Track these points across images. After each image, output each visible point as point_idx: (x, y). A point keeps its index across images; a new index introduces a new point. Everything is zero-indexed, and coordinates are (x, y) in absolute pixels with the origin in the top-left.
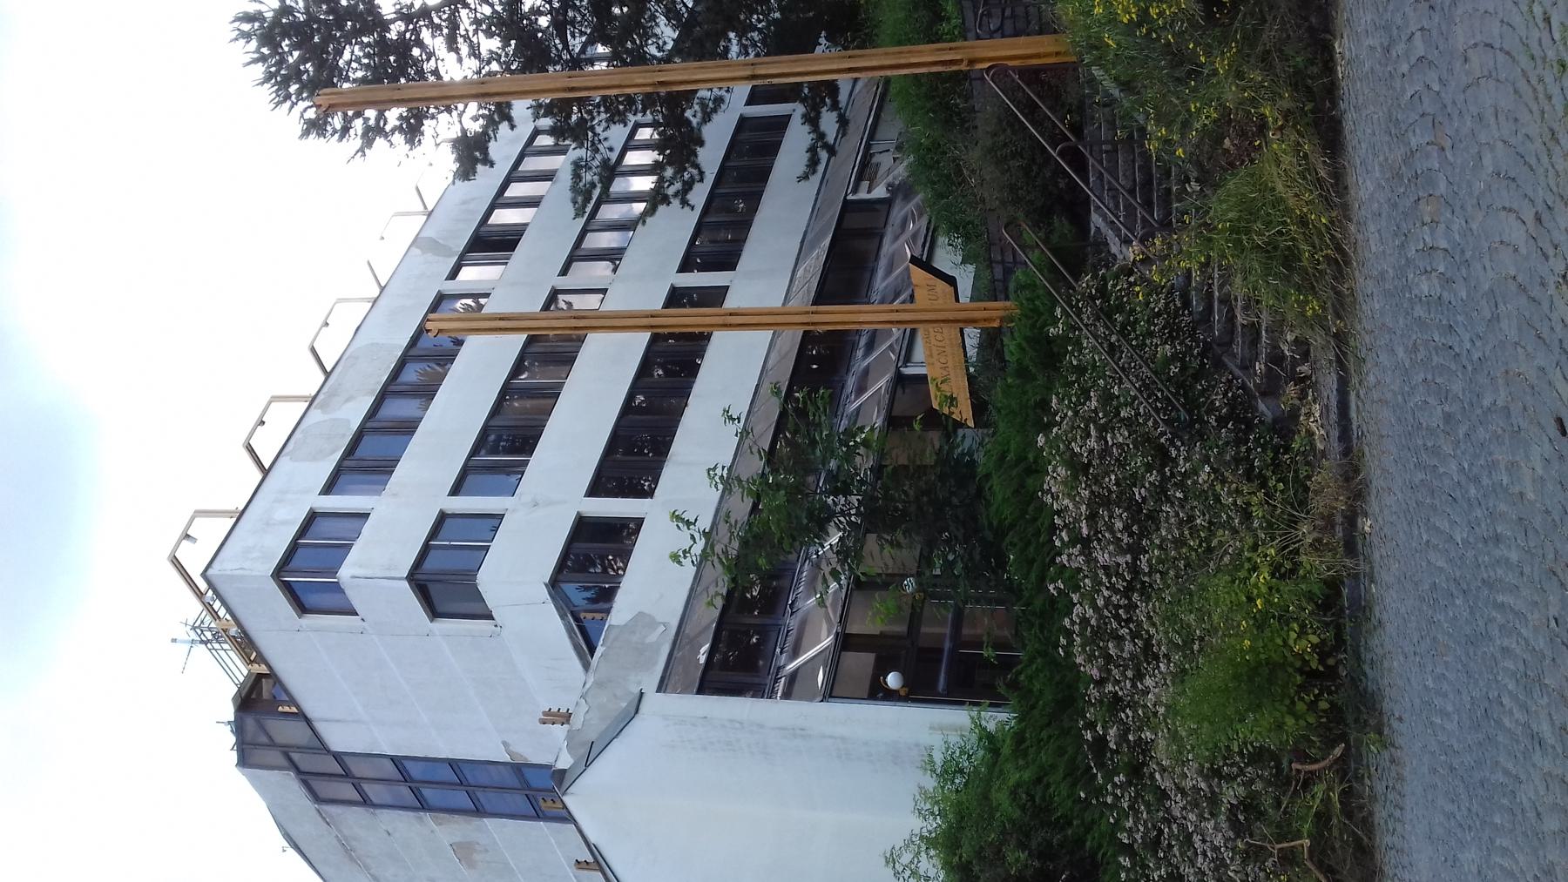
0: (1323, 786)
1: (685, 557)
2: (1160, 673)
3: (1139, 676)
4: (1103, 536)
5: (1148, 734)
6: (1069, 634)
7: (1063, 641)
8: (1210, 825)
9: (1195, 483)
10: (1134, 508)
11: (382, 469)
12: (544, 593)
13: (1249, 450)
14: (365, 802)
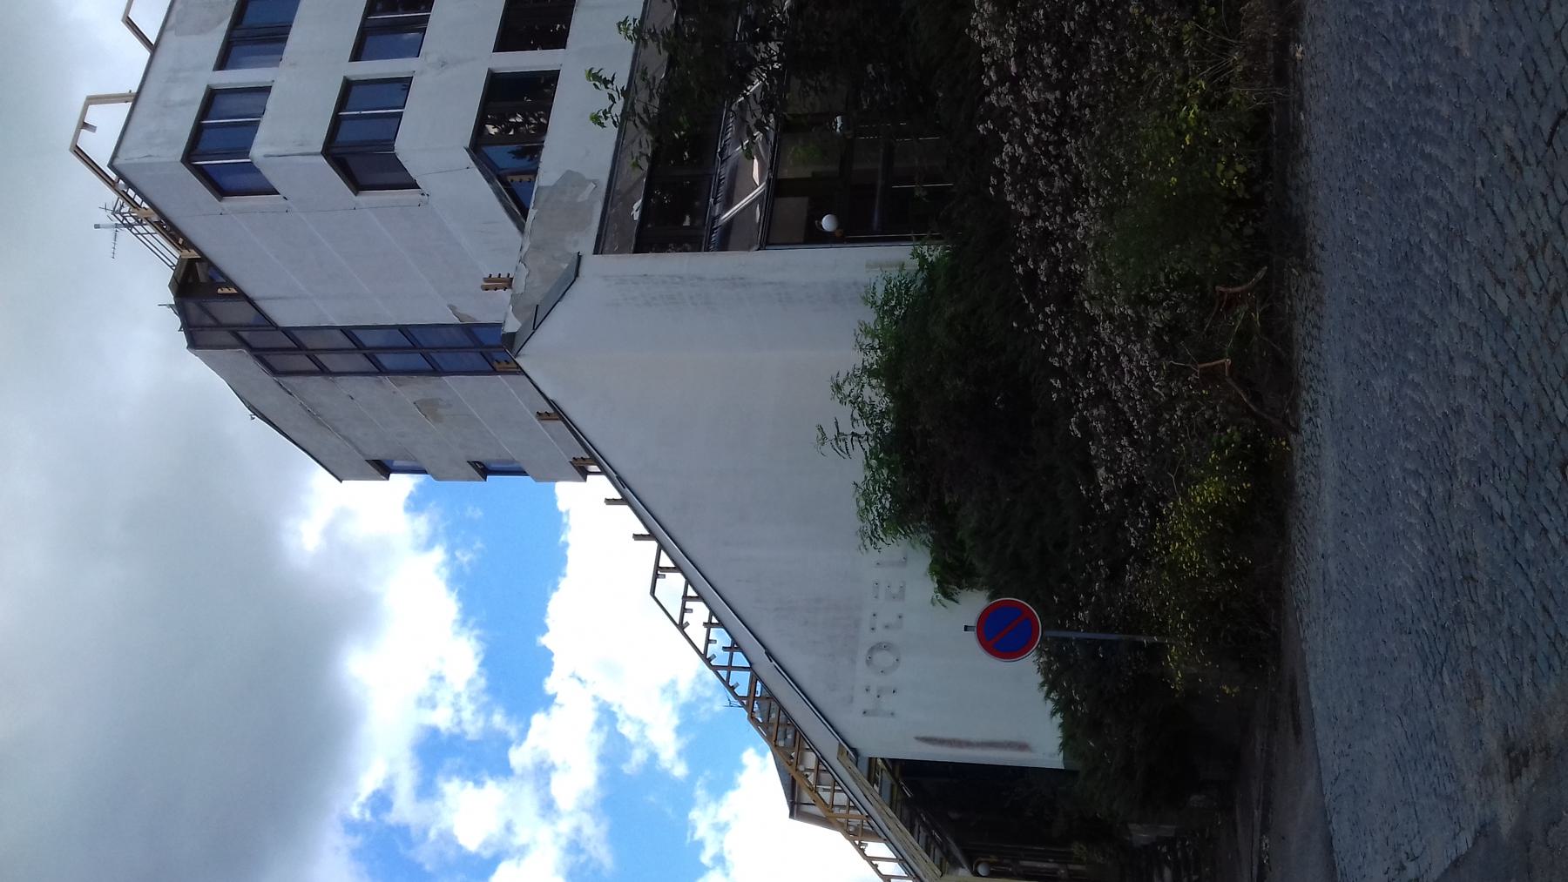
1: (606, 118)
2: (1089, 207)
3: (1070, 210)
4: (1032, 73)
5: (1077, 266)
6: (999, 173)
7: (993, 181)
8: (1136, 348)
9: (1126, 12)
12: (466, 158)
14: (323, 371)
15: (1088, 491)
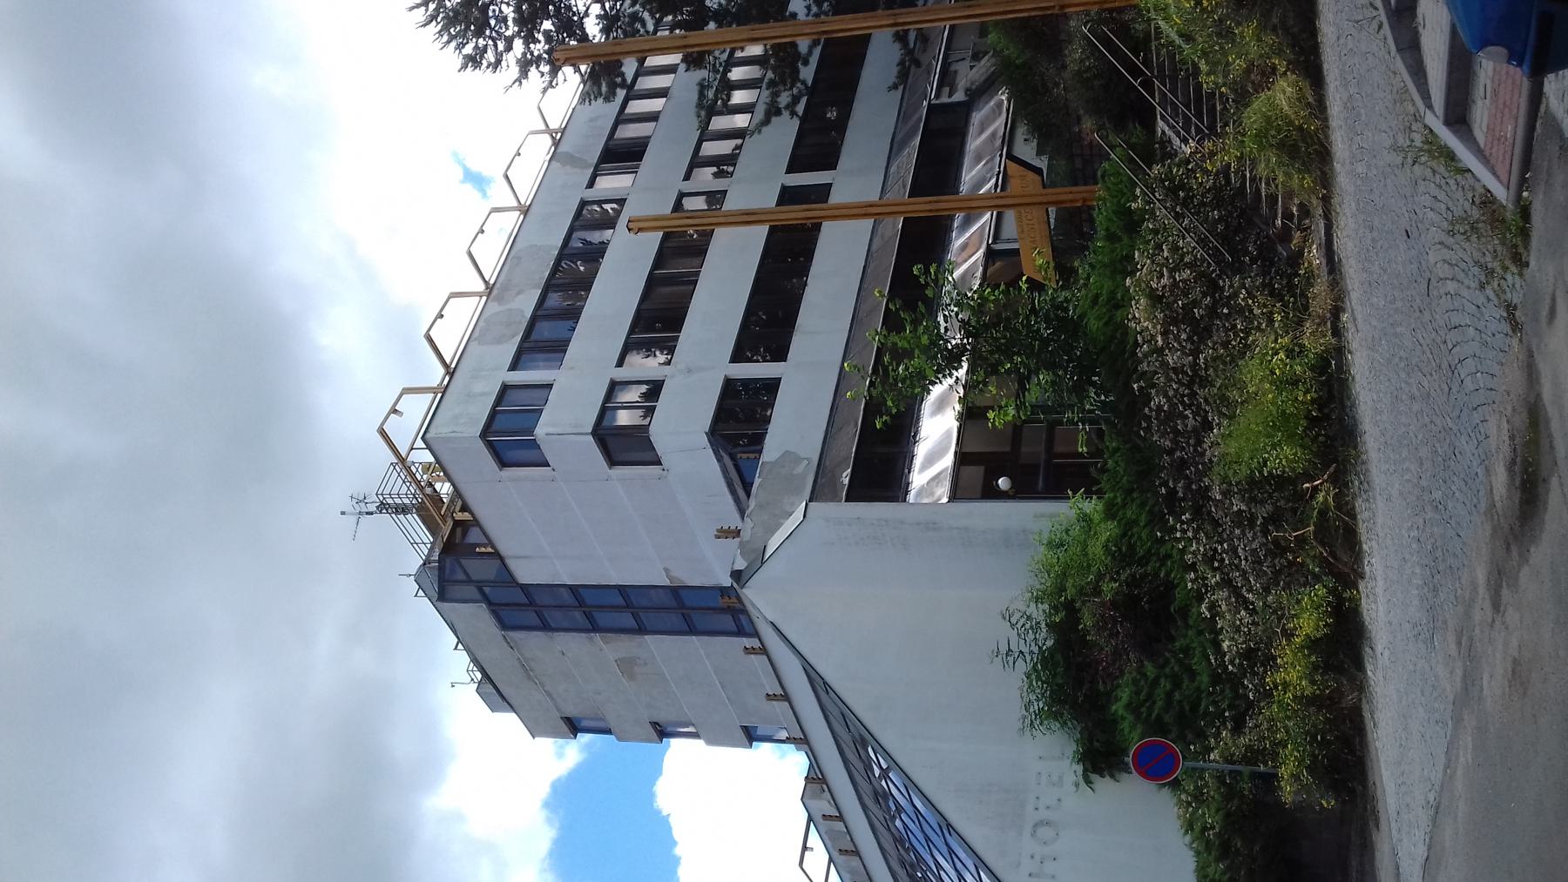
0: (1323, 493)
4: (1173, 346)
7: (1144, 424)
10: (1193, 322)
11: (557, 348)
13: (1271, 279)
15: (1216, 659)
